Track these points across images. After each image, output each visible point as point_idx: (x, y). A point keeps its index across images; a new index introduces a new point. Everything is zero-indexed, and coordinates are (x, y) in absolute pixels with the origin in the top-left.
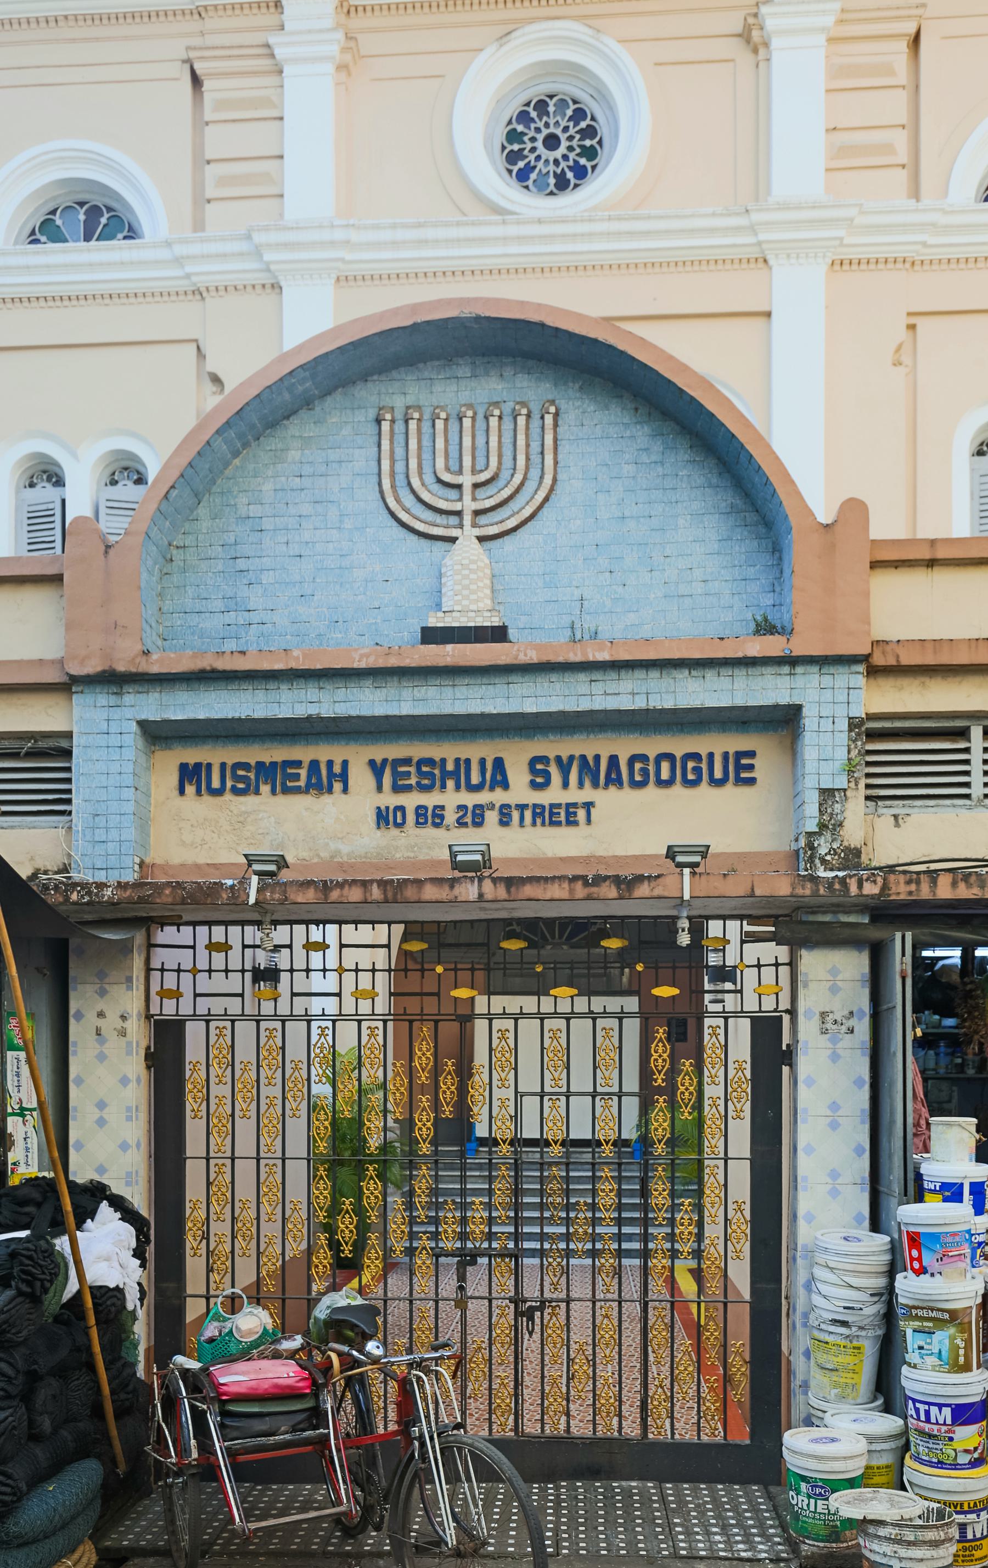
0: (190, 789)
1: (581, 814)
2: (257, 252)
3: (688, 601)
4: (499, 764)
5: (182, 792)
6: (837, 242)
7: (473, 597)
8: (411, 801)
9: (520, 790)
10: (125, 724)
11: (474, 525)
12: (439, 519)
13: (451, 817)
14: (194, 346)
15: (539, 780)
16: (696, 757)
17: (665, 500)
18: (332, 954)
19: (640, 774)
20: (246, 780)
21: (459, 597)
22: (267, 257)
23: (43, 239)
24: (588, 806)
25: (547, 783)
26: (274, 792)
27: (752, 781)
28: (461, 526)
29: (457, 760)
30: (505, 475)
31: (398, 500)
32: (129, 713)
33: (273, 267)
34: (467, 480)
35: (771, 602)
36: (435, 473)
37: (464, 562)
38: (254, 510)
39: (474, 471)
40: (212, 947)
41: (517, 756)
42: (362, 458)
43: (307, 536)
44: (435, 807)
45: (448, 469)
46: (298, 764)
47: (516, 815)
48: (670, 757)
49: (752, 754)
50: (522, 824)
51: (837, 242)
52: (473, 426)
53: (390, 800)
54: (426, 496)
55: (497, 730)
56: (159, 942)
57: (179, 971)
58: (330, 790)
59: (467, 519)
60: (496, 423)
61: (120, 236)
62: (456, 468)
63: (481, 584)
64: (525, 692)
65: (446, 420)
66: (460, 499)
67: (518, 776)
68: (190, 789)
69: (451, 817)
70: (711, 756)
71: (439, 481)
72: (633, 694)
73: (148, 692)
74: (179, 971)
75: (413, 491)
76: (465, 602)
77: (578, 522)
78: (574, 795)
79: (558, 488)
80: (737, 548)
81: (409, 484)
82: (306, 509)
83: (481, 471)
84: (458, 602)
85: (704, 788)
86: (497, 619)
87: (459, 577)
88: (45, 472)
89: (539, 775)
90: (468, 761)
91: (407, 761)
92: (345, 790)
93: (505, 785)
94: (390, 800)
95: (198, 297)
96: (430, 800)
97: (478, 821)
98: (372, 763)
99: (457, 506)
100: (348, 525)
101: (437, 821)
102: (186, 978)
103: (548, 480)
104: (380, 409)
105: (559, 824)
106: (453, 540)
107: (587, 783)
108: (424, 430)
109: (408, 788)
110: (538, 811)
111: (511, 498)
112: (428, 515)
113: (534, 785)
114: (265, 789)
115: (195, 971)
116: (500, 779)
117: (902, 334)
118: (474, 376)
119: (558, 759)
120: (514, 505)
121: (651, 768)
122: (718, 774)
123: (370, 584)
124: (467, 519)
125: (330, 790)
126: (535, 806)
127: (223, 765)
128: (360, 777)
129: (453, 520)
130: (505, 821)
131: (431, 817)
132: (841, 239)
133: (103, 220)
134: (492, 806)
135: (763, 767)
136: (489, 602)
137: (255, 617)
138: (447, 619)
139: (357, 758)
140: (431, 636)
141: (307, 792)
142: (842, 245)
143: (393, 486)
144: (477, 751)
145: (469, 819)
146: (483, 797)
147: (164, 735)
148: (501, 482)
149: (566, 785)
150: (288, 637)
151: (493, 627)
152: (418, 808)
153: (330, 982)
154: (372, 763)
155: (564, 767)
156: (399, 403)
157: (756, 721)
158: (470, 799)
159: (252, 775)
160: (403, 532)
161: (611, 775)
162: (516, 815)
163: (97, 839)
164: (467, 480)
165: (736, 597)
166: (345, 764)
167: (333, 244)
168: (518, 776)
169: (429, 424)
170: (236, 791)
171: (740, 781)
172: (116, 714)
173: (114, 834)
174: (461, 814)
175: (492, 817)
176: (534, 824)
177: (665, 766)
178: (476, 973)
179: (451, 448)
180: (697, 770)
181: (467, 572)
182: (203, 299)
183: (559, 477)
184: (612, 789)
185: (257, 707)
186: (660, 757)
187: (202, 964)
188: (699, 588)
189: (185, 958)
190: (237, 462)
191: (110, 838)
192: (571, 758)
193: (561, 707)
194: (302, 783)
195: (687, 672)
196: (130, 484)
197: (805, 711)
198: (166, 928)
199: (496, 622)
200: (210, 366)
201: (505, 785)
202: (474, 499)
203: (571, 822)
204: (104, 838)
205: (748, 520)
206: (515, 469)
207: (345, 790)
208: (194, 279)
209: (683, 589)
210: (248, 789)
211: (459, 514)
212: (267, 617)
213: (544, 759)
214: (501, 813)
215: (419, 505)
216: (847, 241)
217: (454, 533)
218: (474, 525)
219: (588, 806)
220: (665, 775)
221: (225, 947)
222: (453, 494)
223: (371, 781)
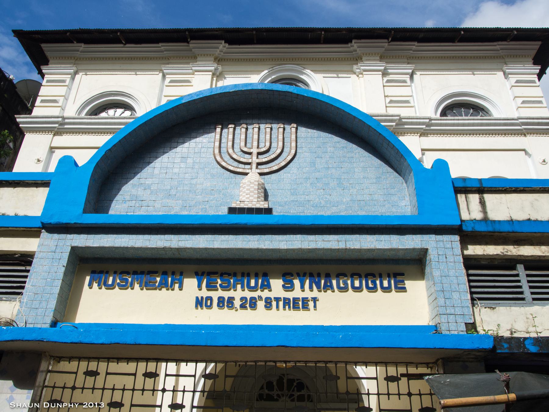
1: (311, 304)
3: (362, 203)
11: (257, 168)
13: (237, 303)
17: (348, 161)
18: (100, 380)
24: (315, 300)
28: (251, 169)
31: (221, 157)
34: (255, 151)
47: (274, 303)
50: (278, 307)
53: (205, 293)
54: (235, 156)
59: (254, 166)
66: (252, 158)
69: (237, 303)
74: (124, 390)
75: (229, 154)
76: (251, 198)
92: (181, 288)
94: (205, 293)
96: (226, 295)
99: (250, 161)
102: (128, 394)
106: (246, 174)
110: (286, 302)
112: (236, 164)
114: (137, 286)
129: (249, 166)
130: (268, 304)
140: (232, 210)
146: (255, 294)
148: (270, 153)
158: (248, 294)
160: (223, 171)
162: (274, 303)
175: (261, 304)
176: (284, 307)
183: (298, 151)
187: (139, 386)
197: (430, 251)
198: (62, 363)
202: (257, 158)
203: (305, 307)
204: (37, 306)
212: (151, 203)
214: (266, 302)
215: (231, 160)
217: (247, 171)
219: (315, 300)
221: (95, 374)
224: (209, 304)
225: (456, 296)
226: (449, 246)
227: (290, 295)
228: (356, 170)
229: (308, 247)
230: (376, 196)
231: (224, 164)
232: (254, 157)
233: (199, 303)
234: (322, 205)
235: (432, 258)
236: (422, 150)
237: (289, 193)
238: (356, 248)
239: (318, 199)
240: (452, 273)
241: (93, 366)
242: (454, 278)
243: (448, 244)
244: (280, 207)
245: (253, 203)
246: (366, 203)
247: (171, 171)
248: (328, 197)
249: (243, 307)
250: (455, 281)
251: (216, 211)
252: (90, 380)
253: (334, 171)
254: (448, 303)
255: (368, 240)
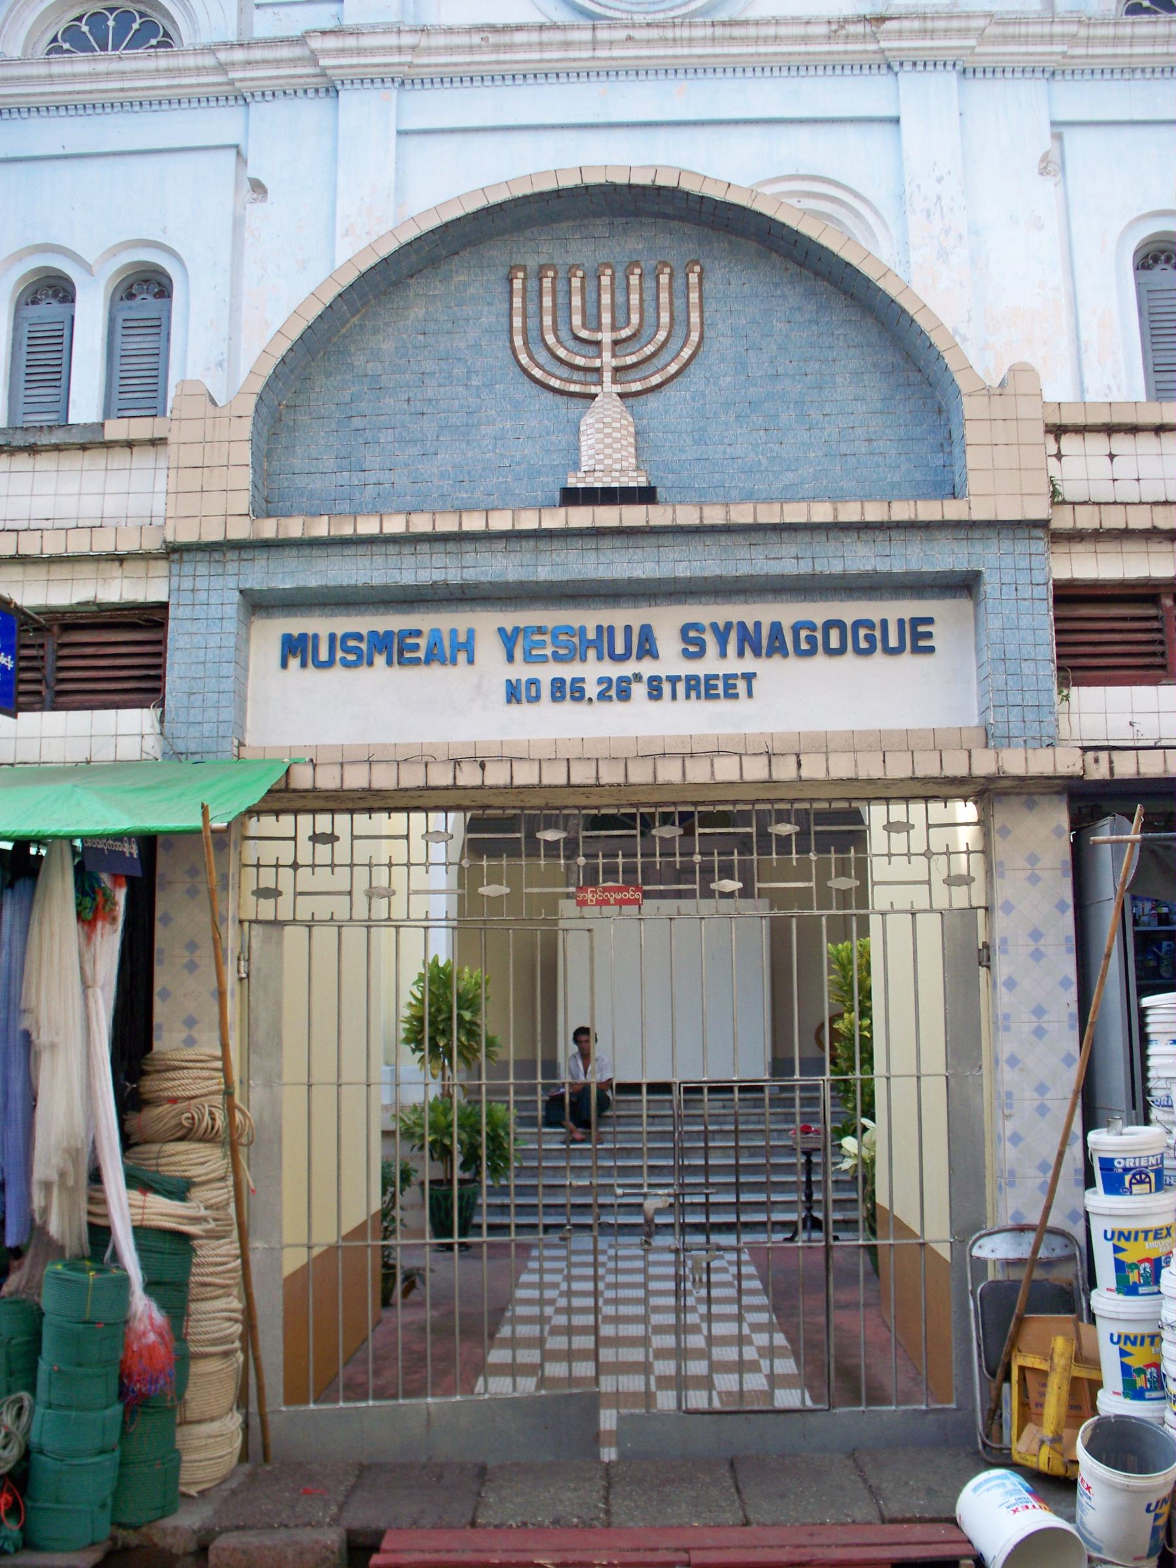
0: (294, 663)
1: (741, 686)
2: (313, 58)
4: (647, 633)
5: (284, 665)
6: (969, 52)
7: (618, 456)
8: (546, 673)
9: (670, 660)
10: (227, 593)
11: (614, 382)
12: (576, 376)
13: (592, 690)
14: (234, 152)
15: (692, 649)
16: (870, 624)
18: (342, 847)
19: (811, 643)
20: (357, 653)
21: (601, 457)
22: (322, 62)
23: (66, 46)
24: (749, 677)
25: (701, 654)
26: (389, 663)
27: (931, 650)
28: (600, 383)
29: (599, 628)
30: (647, 332)
31: (531, 358)
32: (232, 582)
33: (328, 72)
34: (606, 337)
35: (941, 462)
36: (571, 330)
37: (606, 420)
38: (372, 368)
39: (614, 328)
40: (316, 838)
41: (666, 622)
42: (490, 316)
43: (430, 393)
44: (574, 680)
45: (584, 326)
46: (418, 633)
48: (840, 624)
49: (929, 621)
51: (969, 52)
52: (612, 283)
53: (522, 672)
54: (562, 353)
55: (643, 595)
56: (251, 833)
57: (390, 865)
58: (454, 662)
59: (607, 376)
60: (637, 282)
61: (153, 42)
62: (594, 325)
63: (624, 443)
64: (677, 556)
65: (583, 278)
66: (600, 356)
67: (669, 644)
68: (294, 663)
70: (884, 623)
71: (577, 338)
72: (797, 558)
73: (253, 560)
76: (607, 462)
77: (728, 379)
78: (733, 665)
79: (705, 348)
80: (901, 407)
81: (543, 340)
82: (429, 366)
83: (623, 328)
84: (601, 462)
85: (878, 657)
86: (644, 479)
87: (601, 436)
88: (50, 287)
89: (693, 646)
90: (611, 629)
91: (540, 630)
93: (655, 656)
94: (522, 672)
95: (241, 102)
96: (568, 672)
97: (624, 695)
98: (501, 631)
100: (475, 382)
101: (577, 694)
102: (399, 873)
103: (695, 337)
104: (512, 268)
105: (717, 696)
106: (593, 397)
107: (748, 651)
108: (558, 288)
109: (543, 659)
110: (692, 684)
111: (654, 355)
112: (564, 372)
113: (687, 655)
114: (380, 660)
115: (295, 866)
116: (647, 647)
117: (1047, 143)
118: (612, 235)
119: (714, 626)
120: (658, 362)
121: (819, 635)
122: (893, 642)
123: (500, 442)
124: (607, 376)
125: (454, 662)
126: (689, 678)
127: (332, 637)
128: (489, 649)
129: (593, 377)
130: (655, 692)
131: (568, 692)
132: (973, 48)
133: (135, 26)
134: (638, 677)
135: (940, 636)
136: (633, 461)
137: (371, 477)
138: (588, 480)
139: (486, 624)
141: (428, 661)
142: (973, 54)
143: (526, 343)
144: (621, 617)
145: (613, 693)
146: (628, 669)
147: (265, 604)
149: (723, 654)
150: (408, 498)
151: (640, 488)
152: (554, 680)
153: (341, 880)
154: (501, 631)
155: (722, 636)
156: (532, 262)
157: (932, 587)
158: (615, 671)
159: (364, 646)
161: (773, 644)
162: (666, 688)
163: (192, 719)
164: (606, 337)
165: (903, 457)
166: (471, 633)
167: (400, 49)
168: (669, 644)
169: (565, 282)
170: (347, 664)
171: (917, 650)
172: (217, 583)
173: (211, 714)
174: (605, 686)
175: (639, 691)
176: (688, 697)
177: (834, 635)
178: (300, 870)
179: (588, 305)
180: (870, 638)
181: (610, 430)
182: (246, 103)
183: (707, 334)
184: (777, 659)
185: (376, 573)
186: (828, 625)
188: (864, 448)
189: (285, 852)
190: (355, 320)
191: (206, 718)
192: (729, 626)
193: (718, 572)
194: (421, 654)
195: (856, 535)
196: (150, 298)
197: (987, 577)
199: (642, 481)
200: (252, 172)
201: (655, 656)
202: (614, 356)
204: (199, 719)
205: (912, 379)
206: (658, 326)
207: (471, 661)
208: (238, 85)
209: (844, 448)
210: (362, 660)
211: (598, 370)
213: (696, 626)
215: (554, 362)
216: (978, 50)
217: (594, 389)
218: (614, 382)
219: (749, 677)
220: (834, 643)
221: (330, 838)
222: (591, 350)
223: (500, 653)
224: (533, 693)
225: (1028, 668)
226: (1024, 564)
227: (700, 668)
228: (839, 380)
229: (734, 573)
230: (881, 443)
231: (537, 373)
232: (607, 355)
233: (513, 693)
234: (762, 468)
235: (988, 591)
236: (1054, 124)
237: (689, 441)
238: (833, 571)
239: (752, 454)
240: (1025, 621)
241: (323, 823)
242: (1029, 632)
243: (1024, 560)
244: (670, 476)
245: (615, 474)
246: (858, 462)
247: (419, 396)
248: (776, 447)
249: (603, 696)
250: (1030, 639)
251: (529, 488)
252: (323, 850)
253: (788, 382)
254: (1010, 683)
255: (860, 554)
